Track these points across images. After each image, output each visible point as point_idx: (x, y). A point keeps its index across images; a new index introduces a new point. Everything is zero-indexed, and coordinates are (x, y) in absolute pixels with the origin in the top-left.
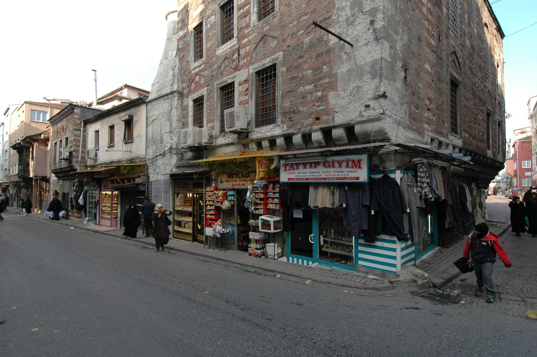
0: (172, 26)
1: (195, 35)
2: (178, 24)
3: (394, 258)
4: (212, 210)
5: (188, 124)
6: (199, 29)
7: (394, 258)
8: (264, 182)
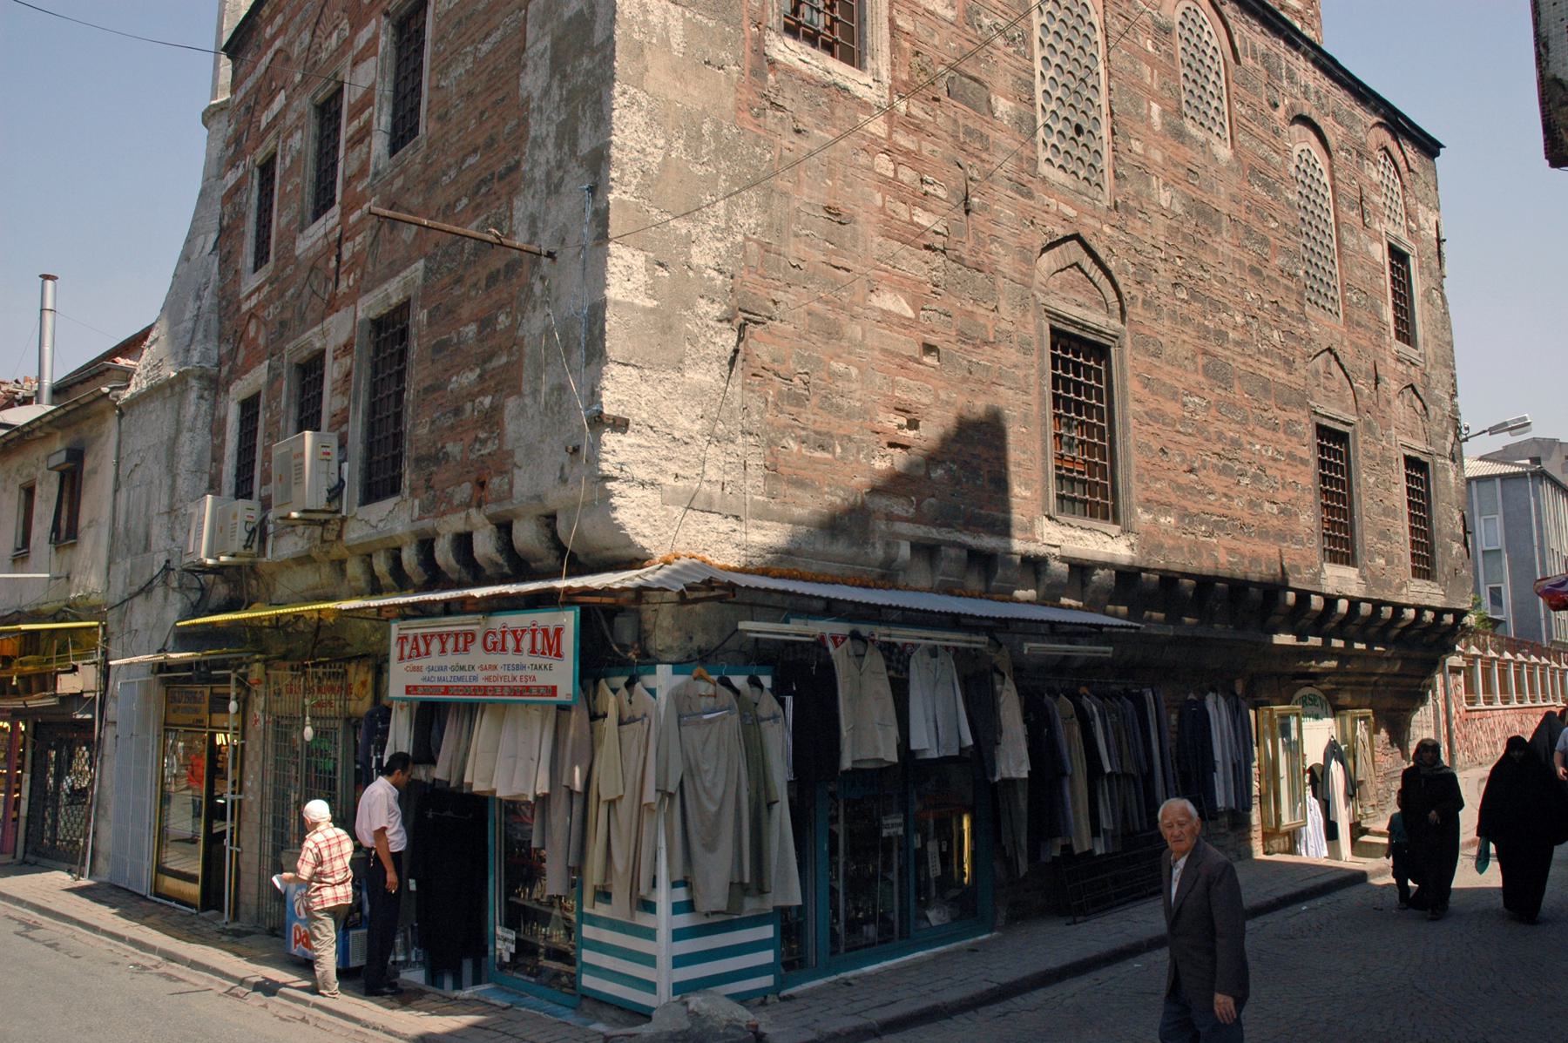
3: (650, 960)
7: (650, 960)
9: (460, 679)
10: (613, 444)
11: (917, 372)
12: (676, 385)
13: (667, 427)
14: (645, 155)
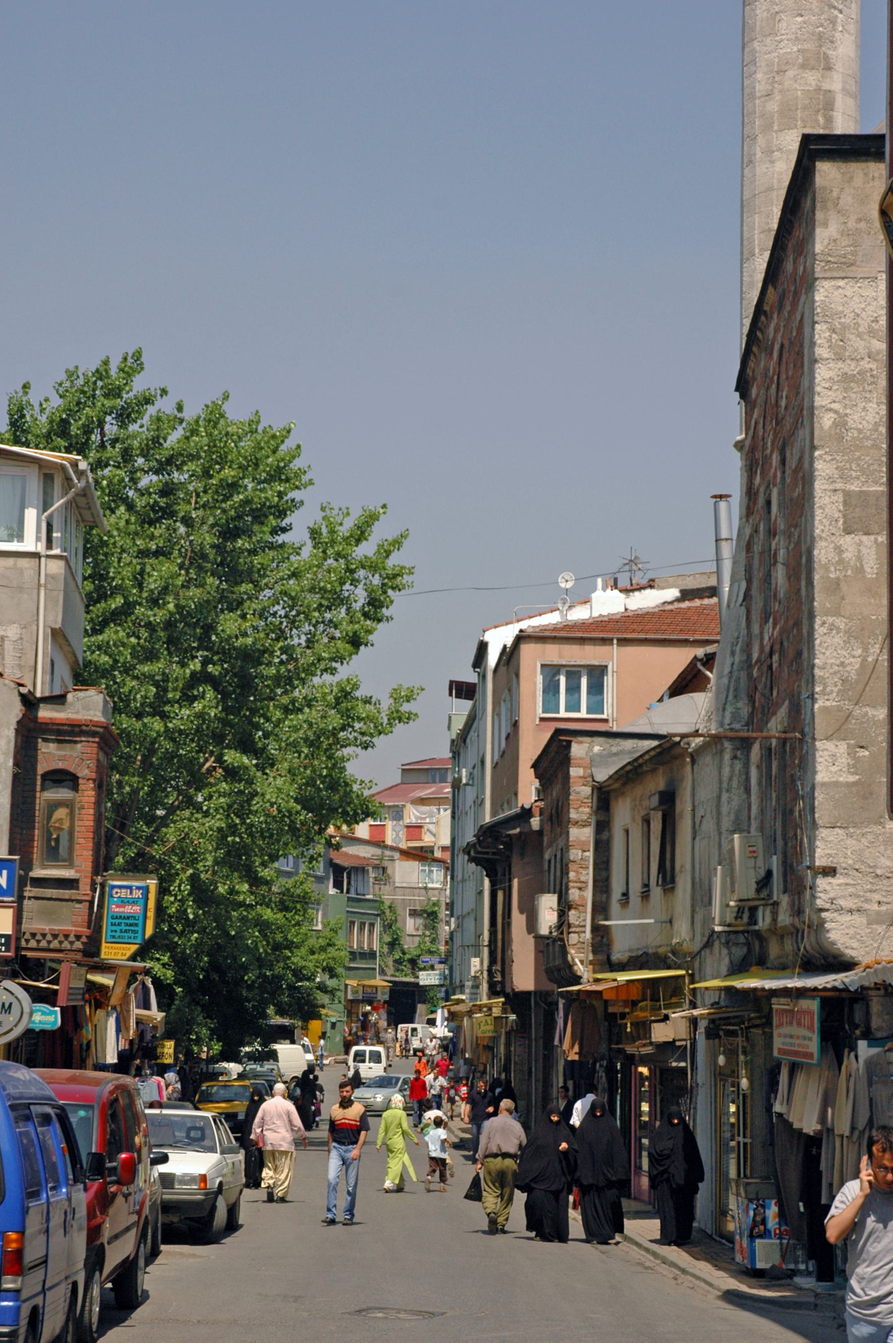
9: (791, 1044)
10: (825, 885)
12: (877, 836)
13: (871, 867)
14: (845, 667)
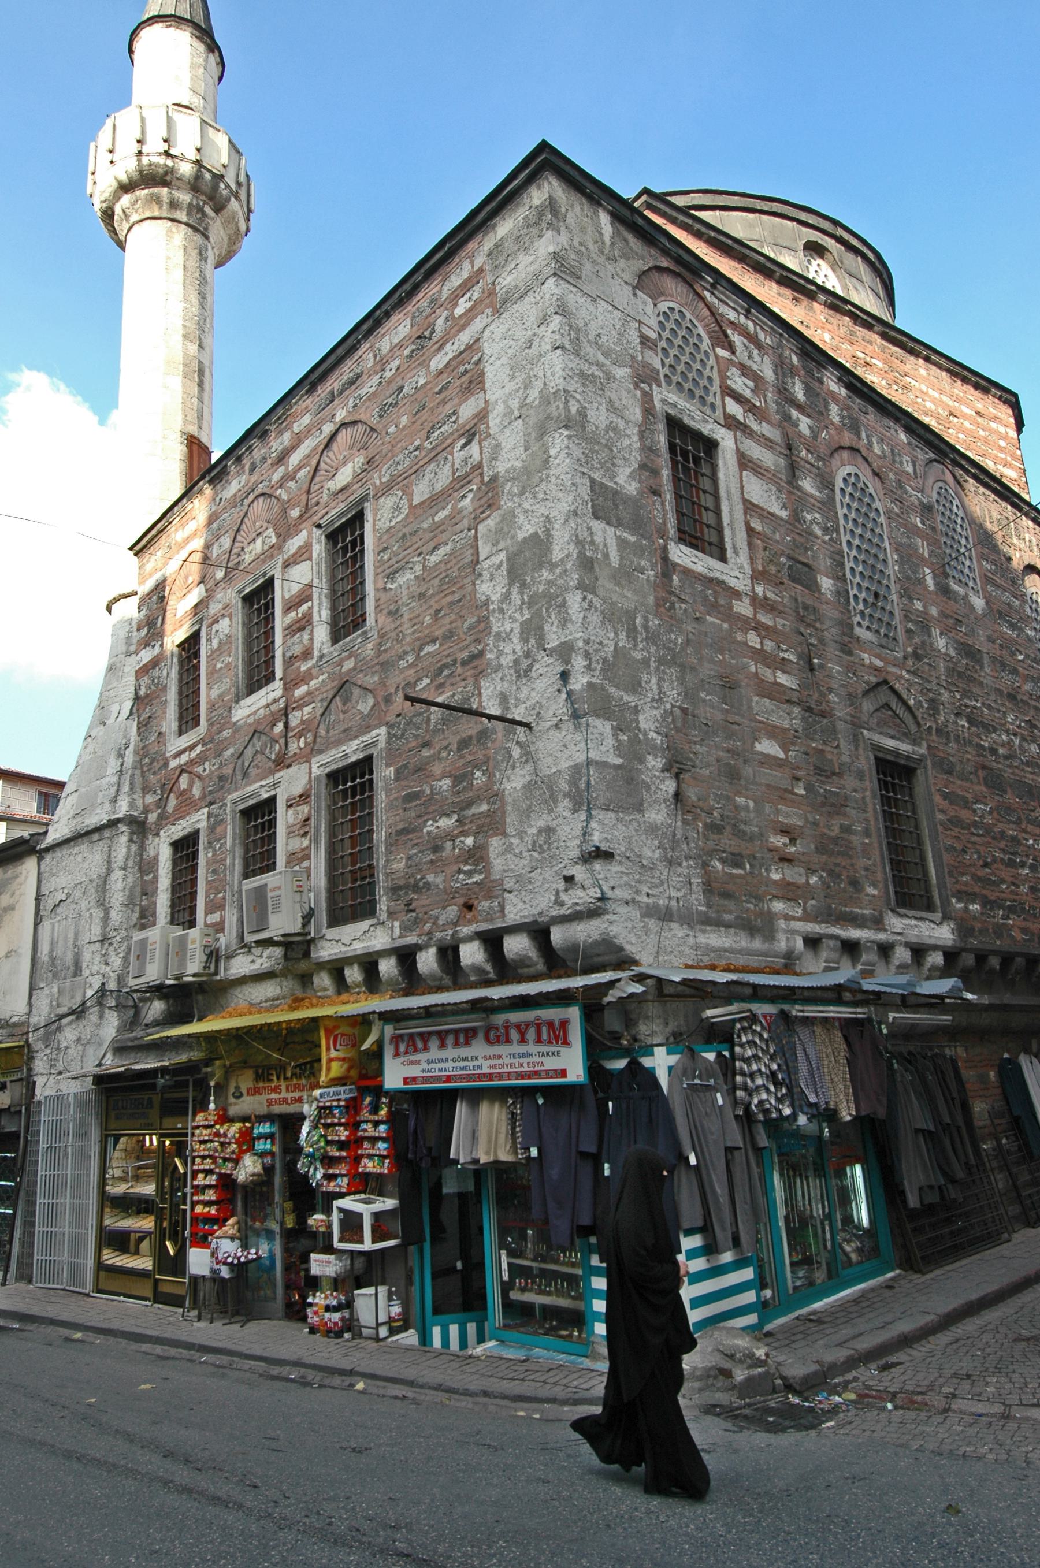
0: (123, 634)
1: (181, 663)
2: (138, 630)
4: (210, 1187)
5: (154, 914)
6: (191, 645)
8: (345, 1093)
11: (793, 801)
